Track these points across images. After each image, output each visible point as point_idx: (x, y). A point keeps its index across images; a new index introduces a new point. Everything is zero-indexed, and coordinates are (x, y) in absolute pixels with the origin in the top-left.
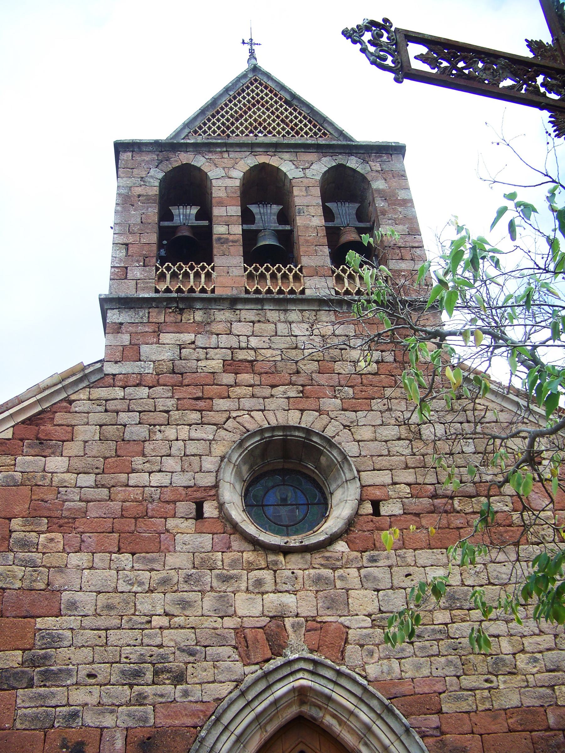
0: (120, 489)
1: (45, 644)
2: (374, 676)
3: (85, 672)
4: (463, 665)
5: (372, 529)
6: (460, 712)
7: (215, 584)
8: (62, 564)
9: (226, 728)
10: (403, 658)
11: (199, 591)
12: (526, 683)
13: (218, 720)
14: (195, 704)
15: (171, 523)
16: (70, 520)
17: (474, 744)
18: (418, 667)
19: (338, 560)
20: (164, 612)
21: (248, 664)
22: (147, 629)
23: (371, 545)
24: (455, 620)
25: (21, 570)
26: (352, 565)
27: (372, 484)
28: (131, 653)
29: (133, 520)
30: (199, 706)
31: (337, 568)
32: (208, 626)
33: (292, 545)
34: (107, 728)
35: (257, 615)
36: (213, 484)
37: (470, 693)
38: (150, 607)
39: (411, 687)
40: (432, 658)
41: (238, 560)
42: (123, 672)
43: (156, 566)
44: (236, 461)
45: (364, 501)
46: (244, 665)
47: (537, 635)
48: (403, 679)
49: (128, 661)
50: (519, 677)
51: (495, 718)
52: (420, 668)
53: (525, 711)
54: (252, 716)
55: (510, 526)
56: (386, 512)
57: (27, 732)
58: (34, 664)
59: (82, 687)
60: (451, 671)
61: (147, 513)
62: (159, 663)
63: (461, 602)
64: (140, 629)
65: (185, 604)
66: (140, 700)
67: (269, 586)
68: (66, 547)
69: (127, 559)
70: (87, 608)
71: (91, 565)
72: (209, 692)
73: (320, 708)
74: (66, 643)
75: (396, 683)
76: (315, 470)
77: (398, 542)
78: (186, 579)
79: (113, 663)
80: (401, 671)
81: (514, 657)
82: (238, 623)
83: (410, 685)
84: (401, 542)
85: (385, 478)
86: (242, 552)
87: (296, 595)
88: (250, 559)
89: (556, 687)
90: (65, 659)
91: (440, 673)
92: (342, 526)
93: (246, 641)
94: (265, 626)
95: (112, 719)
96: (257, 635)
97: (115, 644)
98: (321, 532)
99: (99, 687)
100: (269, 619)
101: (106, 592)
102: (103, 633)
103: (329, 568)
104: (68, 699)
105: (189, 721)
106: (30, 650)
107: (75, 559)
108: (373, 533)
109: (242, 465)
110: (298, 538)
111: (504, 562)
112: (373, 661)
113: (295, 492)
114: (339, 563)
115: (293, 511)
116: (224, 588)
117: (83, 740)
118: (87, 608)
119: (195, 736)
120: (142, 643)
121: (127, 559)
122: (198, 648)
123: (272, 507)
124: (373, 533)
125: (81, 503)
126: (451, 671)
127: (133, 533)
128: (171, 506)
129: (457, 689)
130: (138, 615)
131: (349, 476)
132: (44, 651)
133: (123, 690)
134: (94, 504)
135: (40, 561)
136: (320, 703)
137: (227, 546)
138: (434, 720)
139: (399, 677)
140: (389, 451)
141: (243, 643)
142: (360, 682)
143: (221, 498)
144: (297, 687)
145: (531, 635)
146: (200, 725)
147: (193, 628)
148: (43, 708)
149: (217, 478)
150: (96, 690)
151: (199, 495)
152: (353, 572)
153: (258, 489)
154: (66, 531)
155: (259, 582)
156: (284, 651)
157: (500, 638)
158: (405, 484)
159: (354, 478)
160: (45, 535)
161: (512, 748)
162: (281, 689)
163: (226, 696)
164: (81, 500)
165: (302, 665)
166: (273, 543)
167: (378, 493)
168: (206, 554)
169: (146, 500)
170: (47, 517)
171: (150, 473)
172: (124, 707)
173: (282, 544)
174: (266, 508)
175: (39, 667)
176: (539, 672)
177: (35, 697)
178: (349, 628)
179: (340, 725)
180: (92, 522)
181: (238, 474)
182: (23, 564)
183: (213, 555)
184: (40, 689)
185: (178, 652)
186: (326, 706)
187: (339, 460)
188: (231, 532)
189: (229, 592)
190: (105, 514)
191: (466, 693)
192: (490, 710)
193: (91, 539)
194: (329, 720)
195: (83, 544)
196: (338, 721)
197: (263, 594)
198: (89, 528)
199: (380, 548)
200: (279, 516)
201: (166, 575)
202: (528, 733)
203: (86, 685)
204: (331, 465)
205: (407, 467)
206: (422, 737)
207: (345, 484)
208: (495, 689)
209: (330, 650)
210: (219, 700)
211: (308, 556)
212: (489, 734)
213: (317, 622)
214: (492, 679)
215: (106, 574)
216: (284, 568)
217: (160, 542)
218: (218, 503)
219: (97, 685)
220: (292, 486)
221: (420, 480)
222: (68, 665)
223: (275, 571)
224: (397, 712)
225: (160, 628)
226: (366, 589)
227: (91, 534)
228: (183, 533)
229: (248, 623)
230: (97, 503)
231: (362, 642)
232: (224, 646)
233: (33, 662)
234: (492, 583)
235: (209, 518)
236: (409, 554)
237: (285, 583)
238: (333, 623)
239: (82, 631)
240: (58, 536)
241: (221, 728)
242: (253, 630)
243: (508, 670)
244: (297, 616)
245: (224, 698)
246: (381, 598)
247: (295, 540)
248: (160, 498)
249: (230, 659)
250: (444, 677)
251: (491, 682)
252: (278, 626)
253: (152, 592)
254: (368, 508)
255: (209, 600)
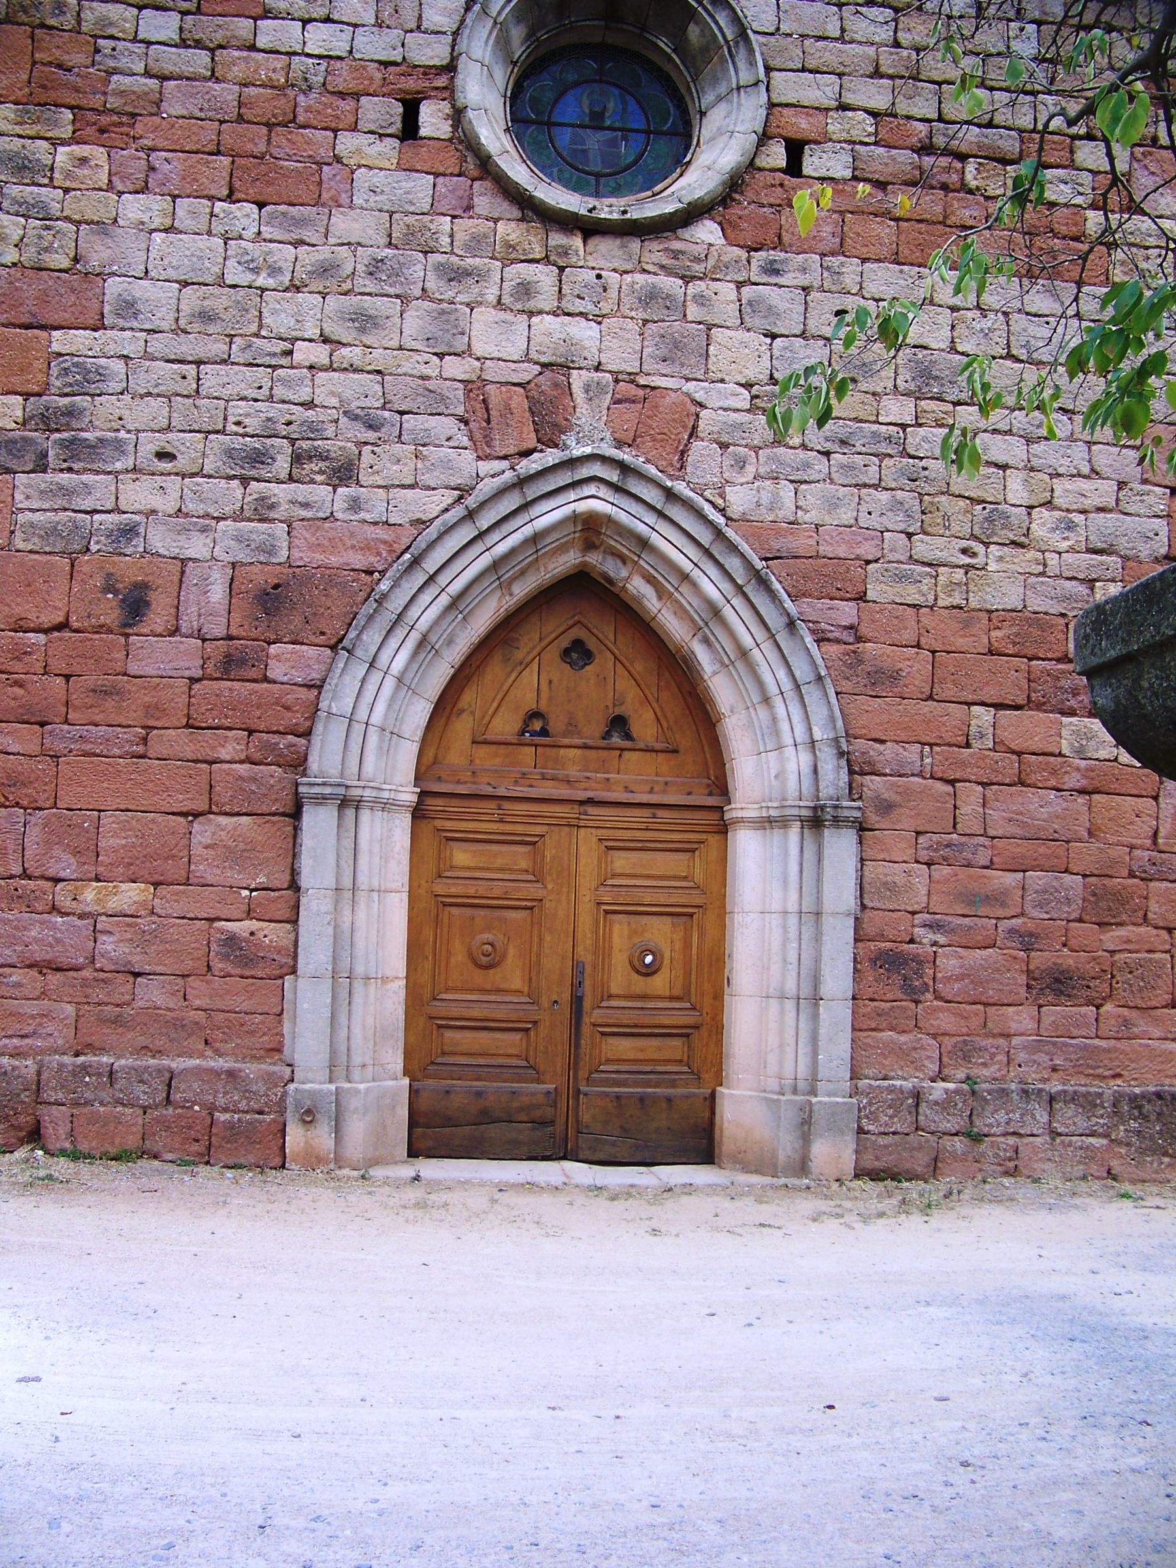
0: (236, 54)
1: (71, 385)
2: (741, 509)
3: (153, 448)
4: (923, 513)
5: (778, 202)
6: (901, 604)
7: (431, 285)
8: (106, 216)
9: (432, 579)
10: (806, 482)
11: (397, 296)
12: (1041, 568)
13: (416, 562)
14: (372, 528)
15: (347, 143)
16: (124, 119)
17: (917, 667)
18: (833, 505)
19: (697, 260)
20: (321, 335)
21: (488, 457)
22: (282, 367)
23: (771, 236)
24: (924, 421)
25: (17, 224)
26: (727, 274)
27: (794, 101)
28: (247, 415)
29: (264, 130)
30: (381, 533)
31: (693, 278)
32: (410, 372)
33: (603, 216)
34: (195, 560)
35: (515, 358)
36: (444, 62)
37: (928, 569)
38: (293, 321)
39: (812, 542)
40: (864, 491)
41: (485, 236)
42: (230, 453)
43: (309, 235)
44: (499, 13)
45: (772, 138)
46: (479, 458)
47: (1085, 477)
48: (798, 524)
49: (241, 431)
50: (1031, 554)
51: (967, 624)
52: (836, 506)
53: (1028, 619)
54: (485, 560)
55: (1076, 239)
56: (815, 170)
57: (37, 556)
58: (48, 425)
59: (145, 477)
60: (896, 521)
61: (295, 117)
62: (303, 439)
63: (943, 385)
64: (269, 366)
65: (365, 322)
66: (263, 511)
67: (546, 299)
68: (114, 179)
69: (248, 216)
70: (159, 315)
71: (168, 222)
72: (402, 506)
73: (623, 560)
74: (115, 386)
75: (784, 529)
76: (674, 56)
77: (830, 237)
78: (371, 269)
79: (209, 432)
80: (797, 507)
81: (1029, 514)
82: (474, 370)
83: (811, 537)
84: (838, 240)
85: (821, 91)
86: (496, 221)
87: (600, 323)
88: (510, 238)
89: (1097, 584)
90: (111, 417)
91: (875, 522)
92: (716, 187)
93: (487, 410)
94: (528, 383)
95: (205, 545)
96: (510, 398)
97: (215, 394)
98: (669, 196)
99: (180, 478)
100: (538, 368)
101: (199, 284)
102: (191, 370)
103: (676, 275)
104: (117, 498)
105: (358, 560)
106: (39, 395)
107: (134, 208)
108: (779, 212)
109: (511, 26)
110: (620, 202)
111: (1047, 316)
112: (743, 480)
113: (624, 103)
114: (698, 268)
115: (613, 143)
116: (449, 294)
117: (146, 579)
118: (159, 315)
119: (369, 590)
120: (272, 396)
121: (248, 216)
122: (387, 414)
123: (570, 129)
124: (779, 212)
125: (147, 81)
126: (896, 521)
127: (262, 158)
128: (347, 105)
129: (903, 558)
130: (264, 337)
131: (745, 77)
132: (67, 400)
133: (228, 489)
134: (177, 86)
135: (59, 206)
136: (625, 551)
137: (465, 204)
138: (847, 612)
139: (792, 519)
140: (843, 30)
141: (481, 413)
142: (711, 517)
143: (458, 95)
144: (582, 514)
145: (1074, 476)
146: (380, 569)
147: (379, 372)
148: (67, 513)
149: (453, 50)
150: (173, 484)
151: (411, 84)
152: (727, 290)
153: (545, 82)
154: (117, 144)
155: (525, 289)
156: (563, 437)
157: (1008, 472)
158: (866, 111)
159: (756, 84)
160: (67, 149)
161: (987, 683)
162: (549, 514)
163: (437, 517)
164: (148, 74)
165: (597, 470)
166: (563, 207)
167: (802, 125)
168: (417, 217)
169: (293, 86)
170: (71, 108)
171: (305, 22)
172: (229, 522)
173: (583, 212)
174: (556, 131)
175: (58, 430)
176: (1071, 550)
177: (51, 491)
178: (702, 405)
179: (660, 598)
180: (173, 126)
181: (503, 43)
182: (22, 210)
183: (431, 221)
184: (61, 475)
185: (344, 420)
186: (636, 559)
187: (730, 37)
188: (475, 173)
189: (461, 304)
190: (201, 110)
191: (920, 569)
192: (961, 608)
193: (169, 166)
194: (638, 586)
195: (152, 175)
196: (656, 591)
197: (531, 314)
198: (167, 139)
199: (790, 245)
200: (584, 152)
201: (328, 256)
202: (1025, 660)
203: (153, 474)
204: (710, 48)
205: (877, 74)
206: (818, 641)
207: (735, 95)
208: (977, 569)
209: (658, 446)
210: (421, 524)
211: (635, 245)
212: (949, 652)
213: (637, 386)
214: (975, 550)
215: (200, 245)
216: (581, 264)
217: (320, 183)
218: (453, 106)
219: (177, 474)
220: (617, 86)
221: (902, 108)
222: (118, 430)
223: (562, 269)
224: (777, 586)
225: (311, 367)
226: (749, 330)
227: (170, 155)
228: (371, 168)
229: (493, 372)
230: (184, 82)
231: (725, 438)
232: (439, 414)
233: (47, 422)
234: (1013, 356)
235: (430, 139)
236: (851, 268)
237: (579, 297)
238: (670, 392)
239: (148, 363)
240: (98, 154)
241: (420, 578)
242: (503, 389)
243: (1011, 537)
244: (597, 368)
245: (432, 521)
246: (776, 353)
247: (611, 206)
248: (324, 84)
249: (451, 444)
250: (882, 532)
251: (975, 555)
252: (556, 385)
253: (298, 289)
254: (777, 156)
255: (418, 317)
